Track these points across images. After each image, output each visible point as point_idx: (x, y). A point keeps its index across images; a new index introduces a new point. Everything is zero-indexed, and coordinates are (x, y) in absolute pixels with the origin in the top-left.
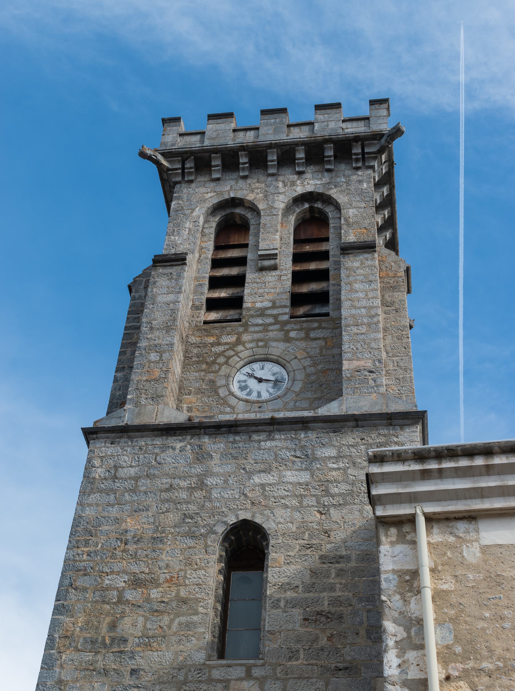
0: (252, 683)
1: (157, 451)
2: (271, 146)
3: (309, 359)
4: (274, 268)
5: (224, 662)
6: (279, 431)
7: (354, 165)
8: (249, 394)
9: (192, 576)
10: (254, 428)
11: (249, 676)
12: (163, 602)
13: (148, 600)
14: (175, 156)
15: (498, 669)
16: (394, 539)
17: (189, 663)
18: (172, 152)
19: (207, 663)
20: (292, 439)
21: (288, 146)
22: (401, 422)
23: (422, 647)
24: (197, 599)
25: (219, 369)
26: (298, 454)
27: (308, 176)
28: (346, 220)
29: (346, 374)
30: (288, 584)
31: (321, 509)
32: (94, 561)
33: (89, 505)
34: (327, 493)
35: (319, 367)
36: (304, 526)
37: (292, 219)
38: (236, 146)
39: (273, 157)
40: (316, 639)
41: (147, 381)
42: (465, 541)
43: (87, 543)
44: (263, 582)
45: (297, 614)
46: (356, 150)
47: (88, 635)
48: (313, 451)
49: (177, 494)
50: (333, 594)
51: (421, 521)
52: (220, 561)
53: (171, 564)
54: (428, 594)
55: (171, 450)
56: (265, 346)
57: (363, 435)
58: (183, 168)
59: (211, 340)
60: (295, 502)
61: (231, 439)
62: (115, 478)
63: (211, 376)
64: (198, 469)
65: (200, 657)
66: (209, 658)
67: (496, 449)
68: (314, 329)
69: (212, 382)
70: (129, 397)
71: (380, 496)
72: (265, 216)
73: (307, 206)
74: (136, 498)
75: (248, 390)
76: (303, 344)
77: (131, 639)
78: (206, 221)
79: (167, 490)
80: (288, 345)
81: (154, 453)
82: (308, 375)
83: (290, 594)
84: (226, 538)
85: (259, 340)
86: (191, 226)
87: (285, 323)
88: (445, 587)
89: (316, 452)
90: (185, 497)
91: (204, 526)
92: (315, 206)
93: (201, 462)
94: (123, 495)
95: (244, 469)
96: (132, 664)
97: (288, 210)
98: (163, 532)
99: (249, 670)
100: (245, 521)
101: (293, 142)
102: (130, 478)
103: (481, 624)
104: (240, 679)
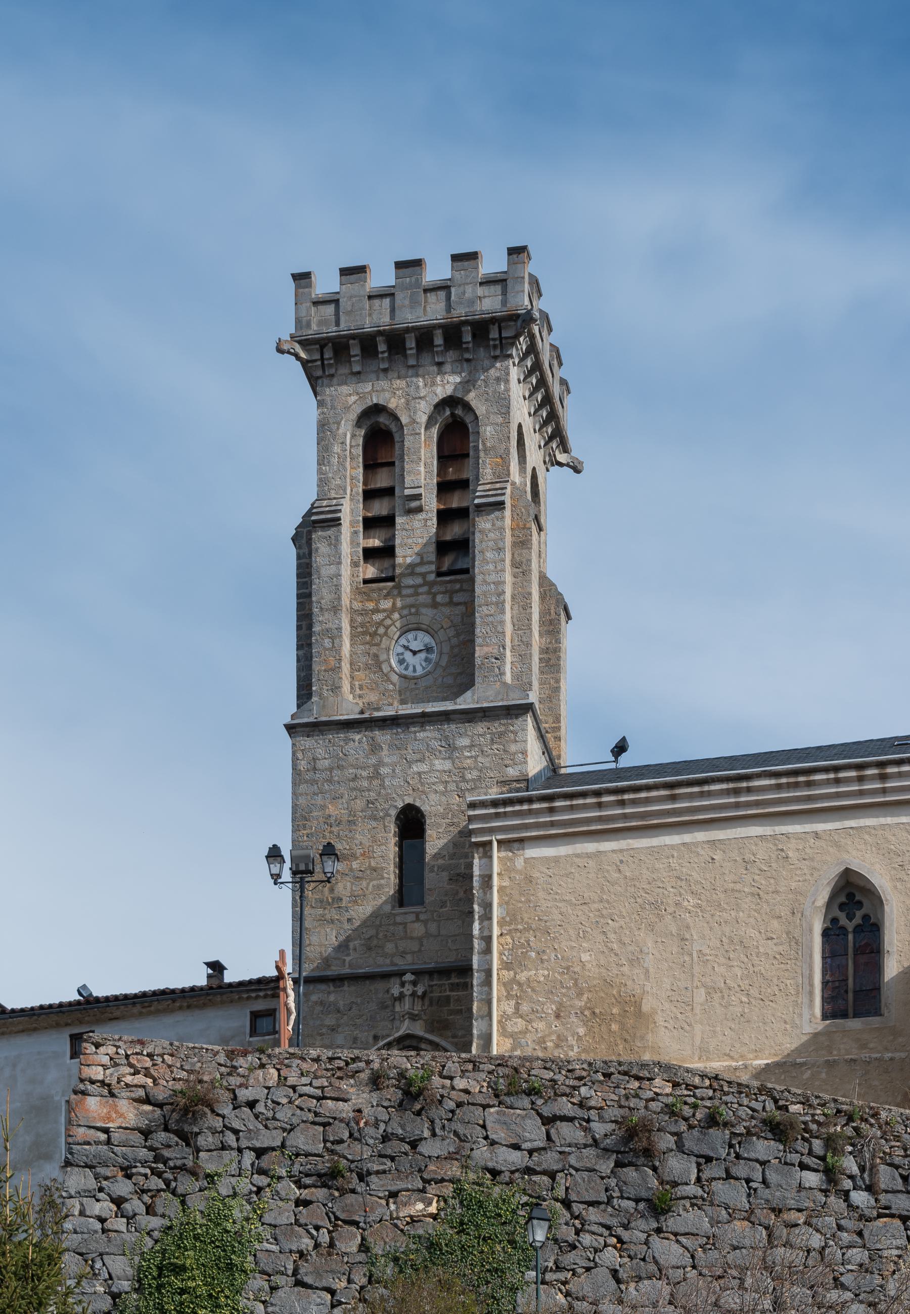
0: (420, 924)
1: (342, 743)
2: (408, 330)
3: (453, 629)
4: (420, 510)
6: (429, 722)
7: (492, 354)
8: (406, 669)
10: (411, 720)
11: (418, 919)
12: (361, 871)
13: (351, 870)
15: (525, 928)
16: (481, 855)
17: (382, 912)
18: (308, 339)
19: (393, 912)
20: (438, 730)
22: (516, 712)
24: (382, 868)
25: (381, 641)
26: (443, 744)
27: (448, 367)
28: (484, 444)
29: (478, 661)
30: (439, 854)
31: (460, 793)
32: (312, 841)
33: (301, 794)
35: (461, 638)
36: (448, 808)
37: (435, 431)
38: (374, 331)
39: (411, 343)
40: (457, 893)
41: (325, 671)
42: (517, 855)
43: (305, 828)
44: (423, 852)
45: (445, 874)
46: (494, 334)
47: (317, 897)
48: (454, 741)
49: (360, 783)
50: (467, 860)
51: (495, 844)
52: (395, 836)
53: (363, 841)
54: (495, 889)
55: (352, 742)
58: (322, 359)
59: (371, 605)
60: (441, 788)
61: (395, 731)
62: (315, 769)
63: (374, 650)
64: (373, 760)
65: (388, 908)
66: (393, 908)
67: (535, 799)
68: (457, 591)
69: (376, 656)
70: (314, 688)
71: (473, 829)
72: (409, 435)
73: (448, 413)
74: (332, 788)
75: (405, 664)
76: (447, 610)
77: (344, 898)
78: (353, 436)
80: (435, 611)
81: (340, 746)
82: (452, 648)
83: (441, 862)
84: (398, 818)
86: (339, 450)
88: (504, 884)
89: (456, 742)
90: (367, 785)
91: (382, 810)
93: (375, 753)
94: (323, 785)
95: (406, 759)
96: (347, 916)
98: (355, 816)
99: (417, 915)
100: (409, 805)
102: (326, 769)
103: (520, 905)
104: (414, 922)
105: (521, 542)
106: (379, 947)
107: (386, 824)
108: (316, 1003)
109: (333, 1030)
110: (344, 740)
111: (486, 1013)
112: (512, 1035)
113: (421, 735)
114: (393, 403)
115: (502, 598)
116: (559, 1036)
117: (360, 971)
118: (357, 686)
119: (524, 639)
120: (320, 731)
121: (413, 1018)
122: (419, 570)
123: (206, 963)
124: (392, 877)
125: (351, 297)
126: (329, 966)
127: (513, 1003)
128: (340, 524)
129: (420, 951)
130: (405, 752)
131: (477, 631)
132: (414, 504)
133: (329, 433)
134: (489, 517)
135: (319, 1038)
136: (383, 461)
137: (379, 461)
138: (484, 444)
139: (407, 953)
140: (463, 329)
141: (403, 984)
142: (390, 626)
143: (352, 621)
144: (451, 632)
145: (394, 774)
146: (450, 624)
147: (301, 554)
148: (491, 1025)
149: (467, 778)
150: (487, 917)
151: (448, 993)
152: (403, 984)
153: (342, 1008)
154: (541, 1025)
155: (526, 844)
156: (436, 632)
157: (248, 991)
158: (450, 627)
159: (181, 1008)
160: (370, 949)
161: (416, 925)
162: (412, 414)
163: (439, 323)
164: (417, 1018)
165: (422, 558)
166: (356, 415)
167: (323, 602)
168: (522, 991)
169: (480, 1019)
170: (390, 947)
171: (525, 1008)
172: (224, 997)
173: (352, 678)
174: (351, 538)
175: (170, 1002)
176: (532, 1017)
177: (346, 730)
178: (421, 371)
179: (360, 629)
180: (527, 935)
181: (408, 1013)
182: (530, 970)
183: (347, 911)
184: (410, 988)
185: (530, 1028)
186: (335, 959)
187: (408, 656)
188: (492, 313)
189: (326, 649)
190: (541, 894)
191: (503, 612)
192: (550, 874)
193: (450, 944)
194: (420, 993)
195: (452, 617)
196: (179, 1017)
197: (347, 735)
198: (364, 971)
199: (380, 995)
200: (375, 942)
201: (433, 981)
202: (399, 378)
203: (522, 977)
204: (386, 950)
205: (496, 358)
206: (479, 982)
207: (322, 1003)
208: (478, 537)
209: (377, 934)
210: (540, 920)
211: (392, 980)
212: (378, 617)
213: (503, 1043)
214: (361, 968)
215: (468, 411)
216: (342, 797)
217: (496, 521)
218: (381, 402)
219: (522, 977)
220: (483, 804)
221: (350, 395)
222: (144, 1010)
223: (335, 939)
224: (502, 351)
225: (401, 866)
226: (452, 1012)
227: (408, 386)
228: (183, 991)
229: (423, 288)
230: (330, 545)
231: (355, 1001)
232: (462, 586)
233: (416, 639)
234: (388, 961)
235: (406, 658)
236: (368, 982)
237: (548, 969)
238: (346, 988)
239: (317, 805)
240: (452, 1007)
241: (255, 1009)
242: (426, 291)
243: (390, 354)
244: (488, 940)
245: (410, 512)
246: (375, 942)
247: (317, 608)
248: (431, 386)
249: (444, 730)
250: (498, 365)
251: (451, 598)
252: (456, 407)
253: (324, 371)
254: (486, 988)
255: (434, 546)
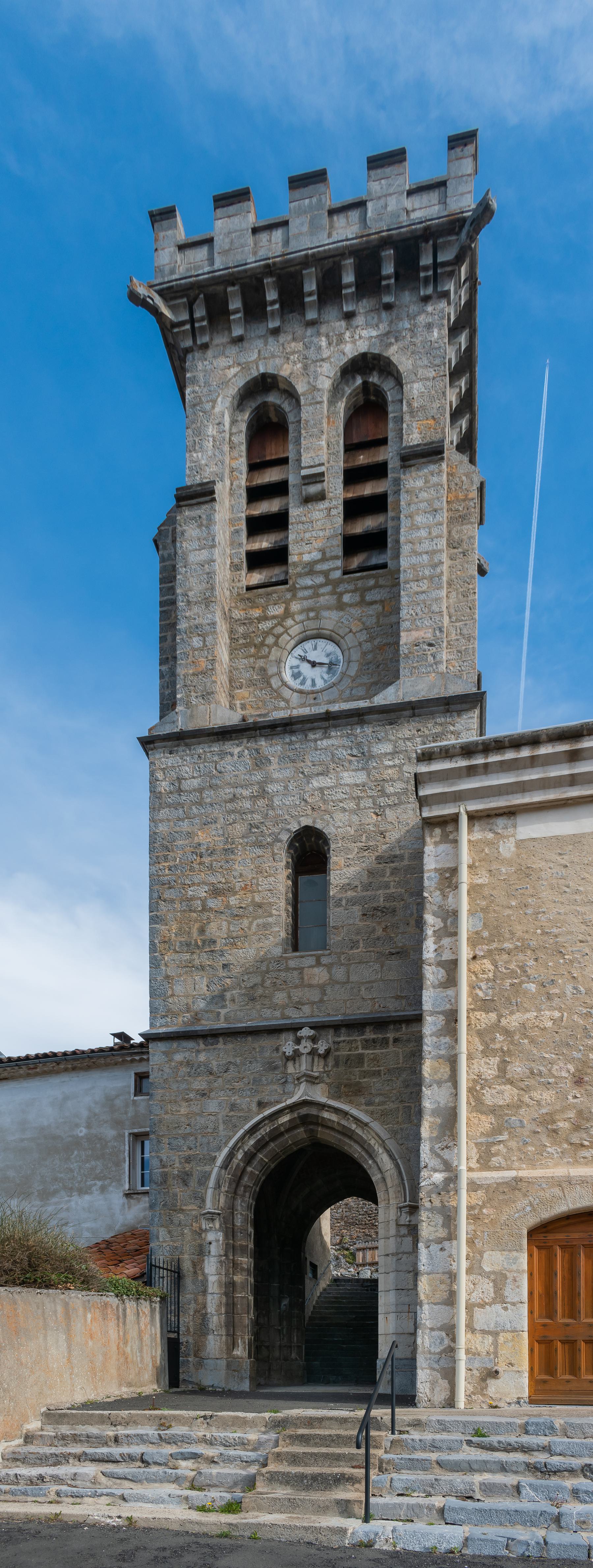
0: (321, 969)
1: (216, 758)
3: (365, 632)
4: (321, 497)
5: (297, 954)
6: (335, 726)
7: (422, 293)
8: (303, 683)
9: (264, 883)
10: (309, 726)
11: (318, 963)
12: (241, 907)
13: (228, 906)
14: (178, 294)
15: (517, 947)
16: (438, 839)
18: (172, 287)
21: (331, 260)
22: (458, 707)
23: (455, 934)
24: (270, 903)
25: (269, 653)
26: (355, 752)
27: (360, 320)
29: (404, 650)
30: (348, 884)
31: (377, 811)
32: (175, 875)
33: (161, 821)
34: (383, 793)
35: (376, 642)
36: (361, 829)
37: (341, 406)
38: (259, 267)
40: (374, 930)
41: (194, 674)
42: (503, 837)
43: (166, 858)
44: (326, 884)
45: (357, 910)
47: (183, 939)
48: (369, 748)
50: (388, 891)
51: (464, 820)
52: (287, 867)
53: (244, 873)
54: (464, 888)
55: (229, 756)
56: (317, 618)
57: (419, 726)
58: (192, 321)
59: (256, 613)
60: (352, 805)
62: (180, 791)
63: (261, 663)
64: (258, 776)
65: (278, 951)
66: (285, 951)
67: (544, 737)
68: (370, 589)
69: (263, 670)
70: (179, 696)
71: (426, 797)
73: (359, 381)
74: (203, 811)
75: (302, 678)
76: (356, 612)
77: (218, 941)
78: (233, 422)
79: (231, 801)
80: (342, 613)
82: (364, 654)
83: (350, 894)
84: (291, 845)
85: (311, 609)
86: (215, 433)
87: (338, 582)
88: (480, 881)
89: (372, 749)
90: (249, 807)
91: (270, 835)
92: (370, 380)
93: (260, 768)
94: (191, 809)
95: (302, 773)
96: (223, 960)
97: (336, 392)
98: (233, 843)
100: (307, 829)
101: (337, 249)
102: (194, 790)
103: (508, 912)
104: (312, 967)
105: (460, 516)
106: (265, 997)
107: (276, 851)
108: (181, 1063)
109: (204, 1095)
110: (219, 755)
111: (446, 1076)
112: (493, 1110)
113: (325, 743)
114: (286, 370)
115: (438, 570)
116: (580, 1113)
117: (240, 1025)
118: (238, 706)
119: (465, 632)
120: (186, 745)
121: (312, 1080)
122: (319, 567)
123: (113, 1034)
124: (284, 914)
125: (229, 233)
126: (199, 1020)
127: (495, 1061)
128: (214, 500)
129: (321, 1001)
130: (302, 764)
131: (403, 613)
132: (313, 489)
133: (201, 414)
134: (421, 473)
135: (184, 1104)
136: (273, 457)
137: (268, 458)
138: (409, 405)
139: (303, 1004)
140: (383, 254)
141: (298, 1041)
142: (282, 634)
143: (231, 632)
144: (363, 637)
145: (286, 792)
146: (361, 626)
147: (166, 555)
148: (456, 1095)
149: (388, 791)
150: (450, 930)
151: (360, 1051)
152: (298, 1041)
153: (215, 1069)
154: (547, 1096)
155: (520, 819)
156: (343, 638)
157: (132, 1054)
158: (361, 630)
159: (66, 1070)
160: (253, 999)
161: (316, 970)
162: (311, 380)
163: (351, 245)
164: (317, 1081)
165: (324, 553)
166: (236, 389)
167: (190, 594)
168: (512, 1043)
169: (435, 1086)
170: (280, 997)
171: (517, 1068)
172: (108, 1060)
173: (232, 697)
174: (231, 538)
175: (55, 1064)
176: (531, 1082)
177: (221, 743)
178: (324, 329)
179: (241, 641)
180: (521, 956)
181: (305, 1075)
182: (527, 1010)
183: (222, 955)
184: (308, 1045)
185: (526, 1099)
186: (207, 1012)
187: (305, 668)
188: (425, 222)
189: (194, 649)
190: (546, 894)
191: (470, 1208)
192: (564, 862)
193: (363, 992)
194: (321, 1051)
195: (364, 619)
196: (64, 1078)
197: (223, 748)
198: (244, 1025)
199: (267, 1054)
200: (260, 991)
201: (339, 1036)
202: (294, 339)
203: (513, 1021)
204: (275, 1001)
205: (426, 299)
206: (434, 1029)
207: (188, 1063)
208: (404, 498)
209: (263, 981)
210: (544, 933)
211: (283, 1036)
212: (266, 625)
213: (476, 1121)
214: (241, 1022)
215: (387, 377)
216: (215, 822)
217: (430, 477)
218: (271, 371)
219: (513, 1021)
220: (446, 753)
221: (229, 367)
222: (30, 1072)
223: (206, 988)
224: (435, 287)
225: (295, 902)
226: (365, 1074)
227: (307, 347)
228: (65, 1054)
229: (327, 208)
230: (200, 526)
231: (233, 1061)
232: (377, 582)
233: (315, 648)
234: (278, 1014)
235: (302, 671)
236: (250, 1038)
237: (560, 1009)
238: (220, 1045)
239: (182, 832)
240: (366, 1067)
241: (139, 1071)
242: (332, 212)
243: (282, 306)
244: (451, 967)
245: (308, 500)
246: (260, 991)
247: (182, 601)
248: (337, 345)
249: (356, 736)
250: (430, 309)
251: (362, 597)
252: (370, 373)
253: (195, 341)
254: (447, 1039)
255: (340, 538)
